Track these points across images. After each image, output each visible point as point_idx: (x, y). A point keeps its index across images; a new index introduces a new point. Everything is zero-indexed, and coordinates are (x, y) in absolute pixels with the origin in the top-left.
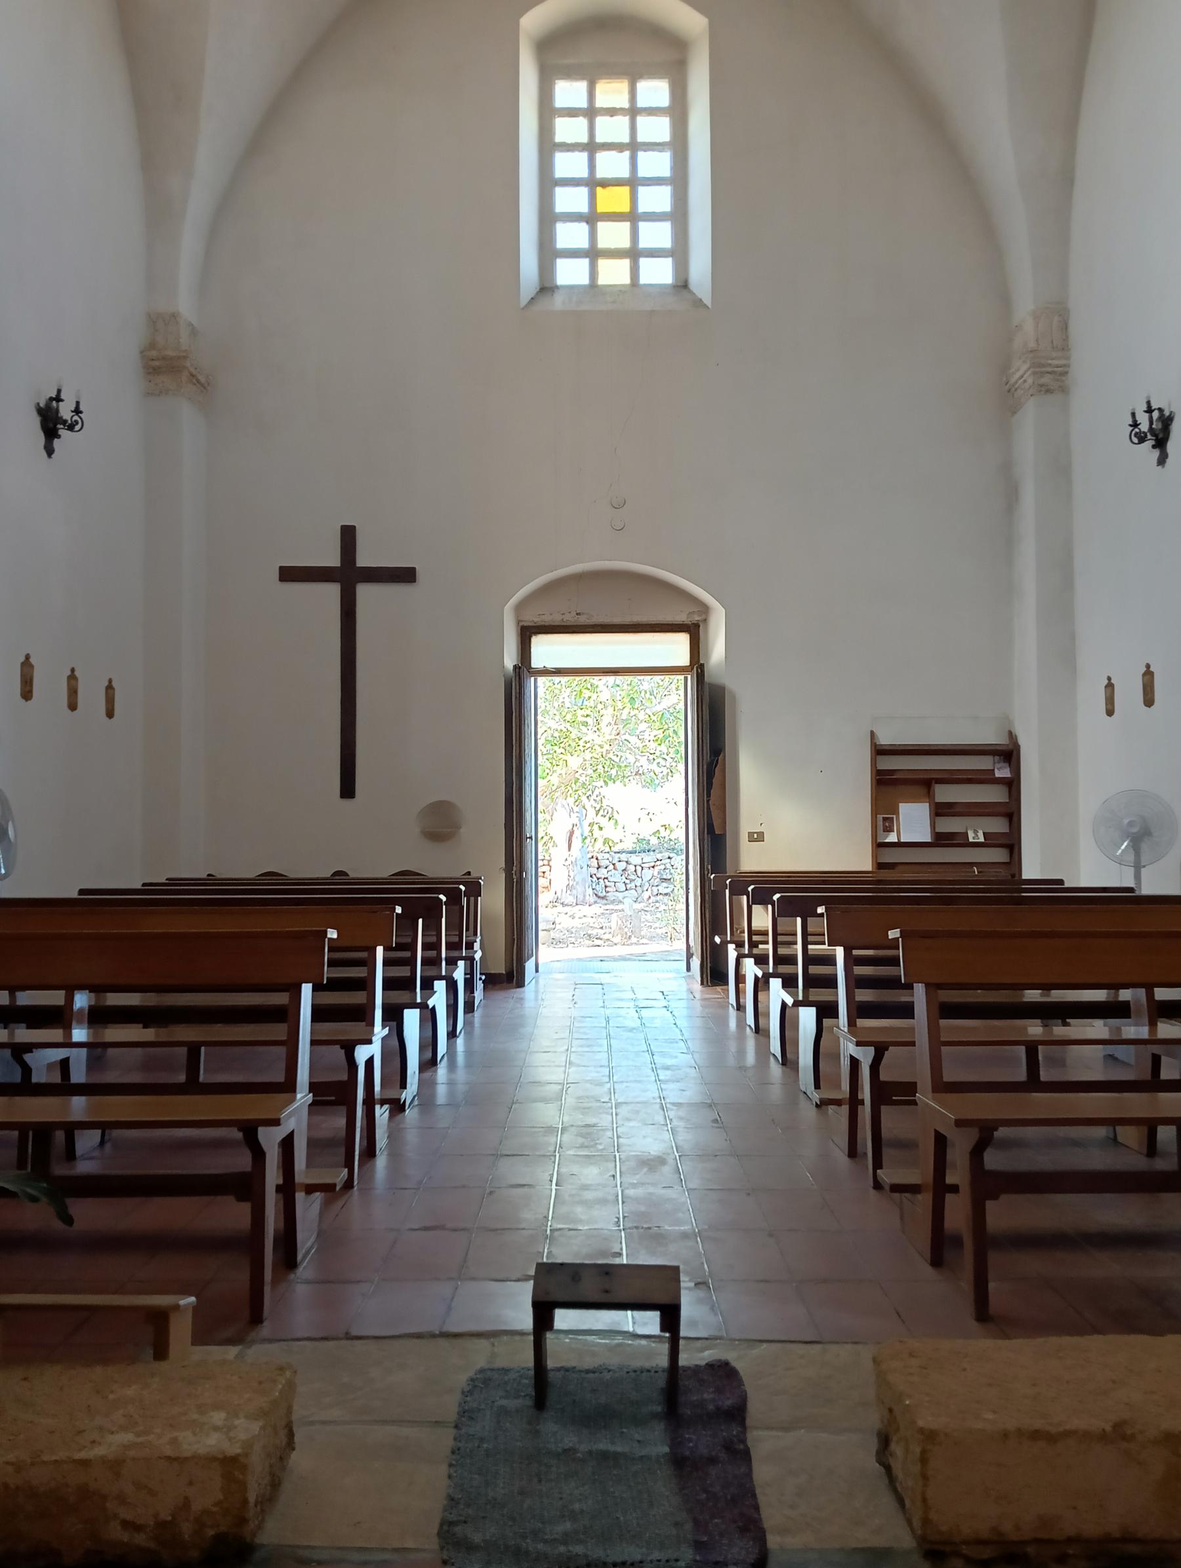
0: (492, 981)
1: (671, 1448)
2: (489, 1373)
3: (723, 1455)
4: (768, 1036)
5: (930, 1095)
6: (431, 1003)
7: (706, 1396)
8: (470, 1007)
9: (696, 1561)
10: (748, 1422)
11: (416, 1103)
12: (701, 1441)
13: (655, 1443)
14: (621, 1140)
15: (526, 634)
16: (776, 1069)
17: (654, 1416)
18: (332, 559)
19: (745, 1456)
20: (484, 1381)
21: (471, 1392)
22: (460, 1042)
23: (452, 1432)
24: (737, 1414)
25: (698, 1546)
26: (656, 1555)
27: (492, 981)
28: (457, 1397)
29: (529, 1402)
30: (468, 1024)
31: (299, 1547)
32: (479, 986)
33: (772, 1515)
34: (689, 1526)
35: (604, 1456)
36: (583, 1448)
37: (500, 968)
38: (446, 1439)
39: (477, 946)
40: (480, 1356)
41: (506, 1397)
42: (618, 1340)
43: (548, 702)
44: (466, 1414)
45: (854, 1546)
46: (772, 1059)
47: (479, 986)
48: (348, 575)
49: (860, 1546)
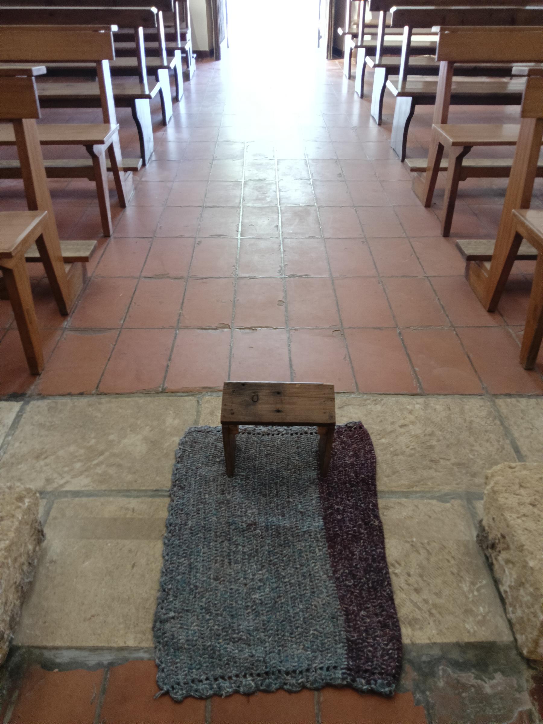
0: (201, 56)
4: (370, 101)
5: (440, 125)
6: (172, 66)
8: (187, 77)
11: (154, 158)
14: (282, 193)
16: (373, 127)
22: (182, 104)
23: (167, 500)
27: (201, 56)
30: (187, 90)
31: (45, 648)
32: (192, 62)
37: (205, 47)
38: (161, 510)
39: (189, 36)
45: (466, 640)
46: (371, 120)
47: (192, 62)
49: (472, 640)
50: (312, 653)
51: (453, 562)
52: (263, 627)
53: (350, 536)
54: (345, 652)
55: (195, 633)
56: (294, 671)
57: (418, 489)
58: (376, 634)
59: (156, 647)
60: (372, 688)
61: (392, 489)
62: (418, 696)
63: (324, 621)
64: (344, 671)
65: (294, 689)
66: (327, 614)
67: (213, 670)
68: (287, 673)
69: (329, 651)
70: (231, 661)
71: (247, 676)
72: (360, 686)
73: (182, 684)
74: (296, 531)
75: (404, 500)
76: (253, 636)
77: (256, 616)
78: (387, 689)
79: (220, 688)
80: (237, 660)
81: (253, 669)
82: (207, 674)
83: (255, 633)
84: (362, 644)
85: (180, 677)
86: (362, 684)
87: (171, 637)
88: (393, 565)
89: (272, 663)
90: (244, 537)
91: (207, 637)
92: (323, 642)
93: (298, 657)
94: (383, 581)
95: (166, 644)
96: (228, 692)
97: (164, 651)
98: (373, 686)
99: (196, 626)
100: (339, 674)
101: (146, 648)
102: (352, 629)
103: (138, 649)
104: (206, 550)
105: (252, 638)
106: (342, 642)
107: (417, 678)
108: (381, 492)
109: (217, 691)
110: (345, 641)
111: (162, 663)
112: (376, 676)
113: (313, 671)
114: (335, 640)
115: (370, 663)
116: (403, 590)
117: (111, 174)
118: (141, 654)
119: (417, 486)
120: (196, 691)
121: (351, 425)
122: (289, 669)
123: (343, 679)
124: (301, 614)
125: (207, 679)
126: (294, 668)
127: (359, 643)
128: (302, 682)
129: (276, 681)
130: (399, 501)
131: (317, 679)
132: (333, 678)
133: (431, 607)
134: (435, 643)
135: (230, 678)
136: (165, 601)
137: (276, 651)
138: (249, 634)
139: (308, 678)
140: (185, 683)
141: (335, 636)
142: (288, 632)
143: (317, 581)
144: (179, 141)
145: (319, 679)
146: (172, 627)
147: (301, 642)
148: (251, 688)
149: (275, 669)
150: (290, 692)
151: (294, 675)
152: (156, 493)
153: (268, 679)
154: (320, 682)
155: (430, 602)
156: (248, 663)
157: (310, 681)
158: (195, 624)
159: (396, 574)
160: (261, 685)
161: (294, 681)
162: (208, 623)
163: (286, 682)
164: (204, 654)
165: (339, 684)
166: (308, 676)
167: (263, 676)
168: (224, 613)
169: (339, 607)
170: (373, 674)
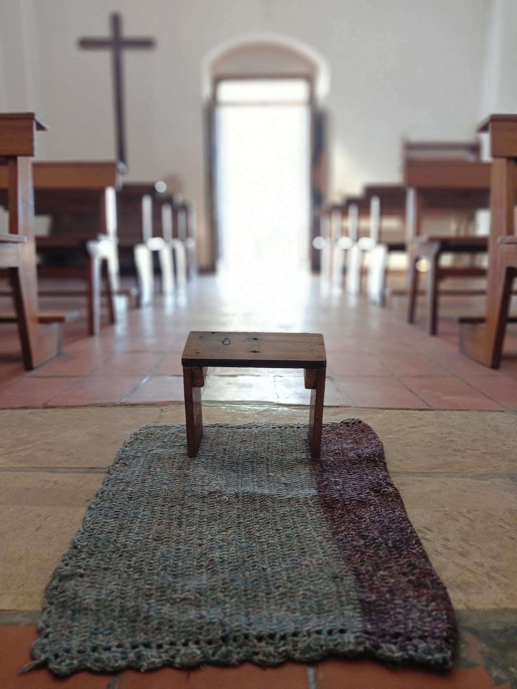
1: (319, 489)
2: (152, 429)
3: (373, 498)
7: (345, 446)
9: (367, 632)
10: (389, 468)
12: (349, 485)
13: (303, 487)
15: (218, 80)
17: (300, 462)
18: (104, 31)
19: (396, 498)
20: (147, 435)
21: (131, 444)
24: (377, 460)
25: (367, 609)
26: (313, 624)
28: (119, 447)
29: (183, 450)
33: (445, 565)
34: (350, 580)
35: (252, 498)
36: (231, 490)
40: (148, 418)
41: (163, 447)
42: (266, 407)
43: (228, 120)
44: (123, 461)
48: (118, 43)
50: (302, 615)
51: (508, 527)
52: (223, 586)
53: (354, 502)
54: (358, 615)
55: (113, 592)
56: (272, 636)
57: (442, 471)
58: (407, 595)
59: (44, 609)
60: (410, 656)
61: (408, 470)
62: (495, 673)
63: (321, 581)
64: (358, 634)
65: (272, 660)
66: (326, 573)
67: (132, 636)
68: (260, 639)
69: (330, 613)
70: (164, 625)
71: (190, 643)
72: (390, 654)
73: (74, 652)
74: (278, 498)
75: (424, 479)
76: (206, 596)
77: (214, 574)
78: (437, 656)
79: (139, 657)
80: (176, 623)
81: (200, 634)
82: (120, 640)
83: (209, 593)
84: (385, 605)
85: (74, 642)
86: (390, 650)
87: (73, 596)
88: (420, 531)
89: (233, 625)
90: (204, 503)
91: (130, 597)
92: (321, 602)
93: (278, 620)
94: (408, 540)
95: (63, 605)
96: (153, 663)
97: (56, 614)
98: (411, 652)
99: (115, 585)
100: (349, 637)
101: (28, 611)
102: (366, 590)
103: (15, 612)
104: (147, 512)
105: (202, 598)
106: (352, 604)
107: (487, 650)
108: (393, 472)
109: (133, 661)
110: (357, 602)
111: (48, 626)
112: (415, 641)
113: (305, 636)
114: (341, 601)
115: (402, 626)
116: (441, 554)
117: (105, 299)
118: (17, 619)
119: (440, 468)
120: (97, 660)
121: (348, 421)
122: (263, 633)
123: (358, 644)
124: (284, 573)
125: (119, 646)
126: (272, 632)
127: (380, 605)
128: (285, 651)
129: (238, 650)
130: (420, 479)
131: (312, 645)
132: (338, 644)
133: (490, 570)
134: (506, 609)
135: (160, 646)
136: (74, 558)
137: (243, 613)
138: (199, 593)
139: (295, 644)
140: (79, 652)
141: (340, 597)
142: (262, 592)
143: (308, 542)
144: (176, 306)
145: (315, 645)
146: (77, 586)
147: (284, 603)
148: (194, 657)
149: (238, 634)
150: (263, 665)
151: (270, 641)
152: (91, 470)
153: (226, 646)
154: (316, 650)
155: (486, 565)
156: (193, 626)
157: (300, 649)
158: (114, 583)
159: (427, 539)
160: (213, 655)
161: (271, 649)
162: (135, 583)
163: (257, 650)
164: (120, 617)
165: (351, 651)
166: (297, 642)
167: (217, 643)
168: (163, 573)
169: (344, 566)
170: (410, 639)
